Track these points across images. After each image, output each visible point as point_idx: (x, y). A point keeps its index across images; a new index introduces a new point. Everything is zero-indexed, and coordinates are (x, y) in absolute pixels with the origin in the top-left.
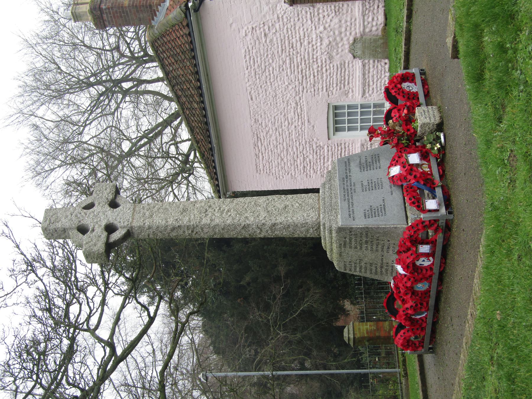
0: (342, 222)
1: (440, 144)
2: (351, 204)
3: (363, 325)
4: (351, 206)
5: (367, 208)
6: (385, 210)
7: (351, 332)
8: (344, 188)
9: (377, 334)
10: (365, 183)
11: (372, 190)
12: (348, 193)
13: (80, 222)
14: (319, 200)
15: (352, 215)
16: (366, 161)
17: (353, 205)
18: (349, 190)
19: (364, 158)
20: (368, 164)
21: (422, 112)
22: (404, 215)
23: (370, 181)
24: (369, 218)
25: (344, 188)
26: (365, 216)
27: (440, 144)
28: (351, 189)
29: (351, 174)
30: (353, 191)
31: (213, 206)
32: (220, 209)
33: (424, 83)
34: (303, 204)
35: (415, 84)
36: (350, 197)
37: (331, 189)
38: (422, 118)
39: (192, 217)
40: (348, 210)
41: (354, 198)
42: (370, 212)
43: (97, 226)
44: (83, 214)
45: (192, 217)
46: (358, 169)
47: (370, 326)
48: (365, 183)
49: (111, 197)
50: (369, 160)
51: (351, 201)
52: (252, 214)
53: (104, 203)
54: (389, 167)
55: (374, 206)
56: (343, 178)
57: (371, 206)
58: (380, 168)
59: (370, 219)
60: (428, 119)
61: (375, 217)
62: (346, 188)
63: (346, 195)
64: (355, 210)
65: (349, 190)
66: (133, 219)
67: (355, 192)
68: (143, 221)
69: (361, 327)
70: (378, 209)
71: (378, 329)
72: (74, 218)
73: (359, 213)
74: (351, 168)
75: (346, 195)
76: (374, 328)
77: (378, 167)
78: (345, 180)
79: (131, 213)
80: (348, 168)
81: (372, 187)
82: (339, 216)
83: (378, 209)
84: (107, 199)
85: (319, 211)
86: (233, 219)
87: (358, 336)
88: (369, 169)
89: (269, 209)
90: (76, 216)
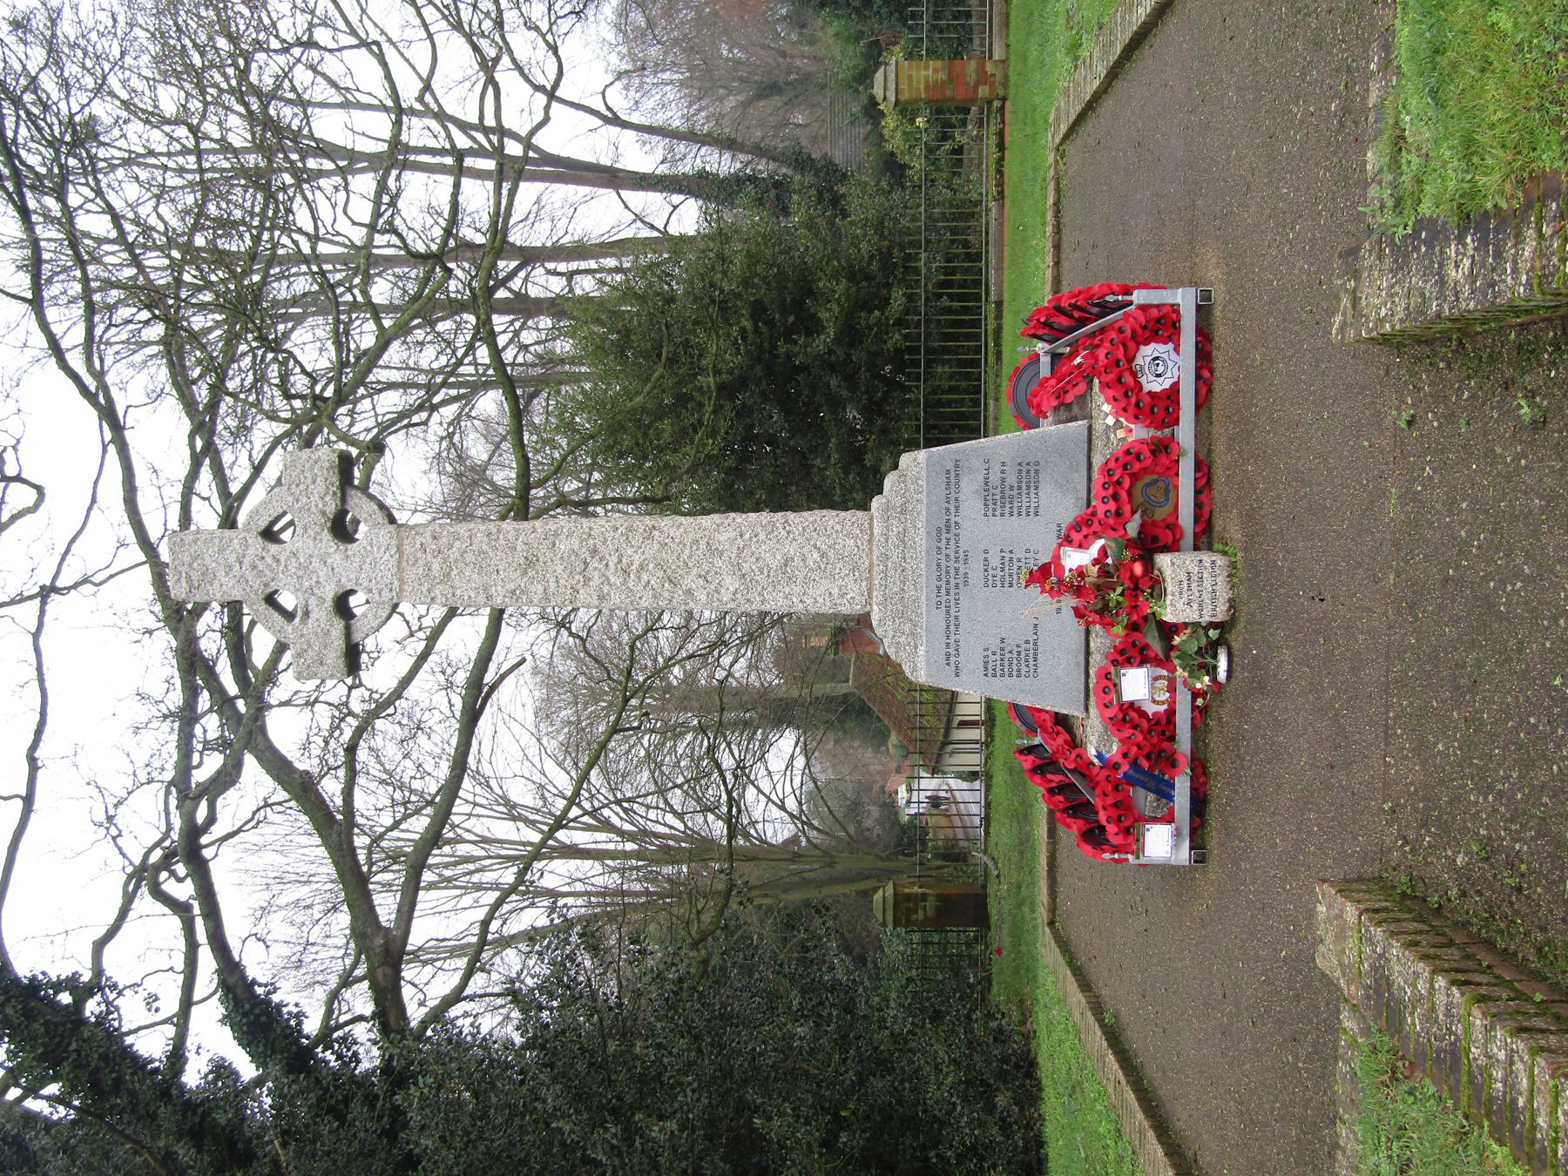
0: (929, 675)
1: (1214, 679)
2: (952, 624)
3: (918, 69)
4: (952, 628)
5: (994, 644)
6: (1035, 654)
7: (892, 87)
8: (939, 565)
9: (948, 93)
10: (995, 561)
11: (1011, 585)
12: (948, 583)
13: (266, 585)
14: (870, 541)
15: (953, 659)
16: (1003, 480)
17: (957, 626)
18: (952, 572)
19: (998, 468)
20: (1007, 493)
21: (1184, 578)
22: (1082, 687)
23: (1007, 555)
24: (994, 675)
25: (939, 565)
26: (986, 669)
27: (1214, 679)
28: (957, 570)
29: (958, 519)
30: (961, 581)
31: (602, 549)
32: (620, 561)
33: (1204, 357)
34: (831, 554)
35: (1177, 350)
36: (952, 598)
37: (903, 541)
38: (1180, 606)
39: (552, 585)
40: (944, 640)
41: (964, 603)
42: (998, 657)
43: (313, 602)
44: (269, 560)
45: (552, 585)
46: (980, 504)
47: (936, 71)
48: (995, 561)
49: (331, 509)
50: (1012, 479)
51: (953, 610)
52: (701, 581)
53: (318, 529)
54: (1060, 545)
55: (1010, 645)
56: (939, 530)
57: (1002, 640)
58: (1036, 514)
59: (998, 680)
60: (1195, 606)
61: (1011, 675)
62: (943, 563)
63: (943, 591)
64: (962, 643)
65: (952, 572)
66: (402, 581)
67: (966, 583)
68: (429, 591)
69: (914, 74)
70: (1019, 653)
71: (951, 80)
72: (249, 575)
73: (971, 658)
74: (962, 497)
75: (943, 591)
76: (942, 76)
77: (1032, 510)
78: (944, 536)
79: (393, 561)
80: (953, 495)
81: (1011, 575)
82: (922, 650)
83: (1019, 653)
84: (324, 513)
85: (870, 579)
86: (654, 596)
87: (905, 96)
88: (1007, 510)
89: (746, 568)
90: (254, 567)
